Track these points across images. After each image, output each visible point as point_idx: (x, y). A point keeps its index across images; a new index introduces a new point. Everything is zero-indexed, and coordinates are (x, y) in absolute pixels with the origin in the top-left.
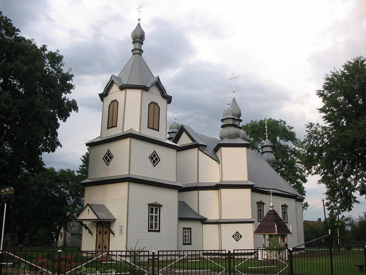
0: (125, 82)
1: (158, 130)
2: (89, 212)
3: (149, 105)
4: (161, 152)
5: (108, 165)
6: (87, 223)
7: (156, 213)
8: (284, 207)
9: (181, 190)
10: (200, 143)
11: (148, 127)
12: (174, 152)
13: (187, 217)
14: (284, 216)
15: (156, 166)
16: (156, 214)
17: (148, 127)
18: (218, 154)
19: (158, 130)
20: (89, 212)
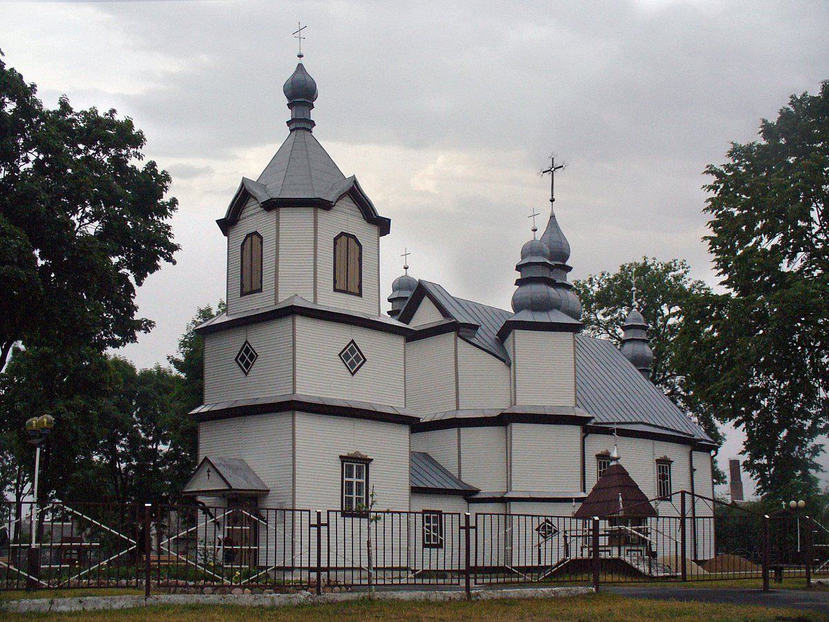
0: (276, 191)
1: (360, 295)
2: (209, 475)
3: (335, 239)
4: (365, 339)
5: (246, 374)
6: (207, 501)
7: (359, 476)
8: (664, 465)
9: (416, 426)
10: (462, 320)
11: (335, 290)
12: (399, 341)
13: (430, 486)
14: (664, 484)
15: (356, 374)
16: (360, 478)
17: (335, 290)
18: (508, 343)
19: (360, 295)
20: (209, 475)
